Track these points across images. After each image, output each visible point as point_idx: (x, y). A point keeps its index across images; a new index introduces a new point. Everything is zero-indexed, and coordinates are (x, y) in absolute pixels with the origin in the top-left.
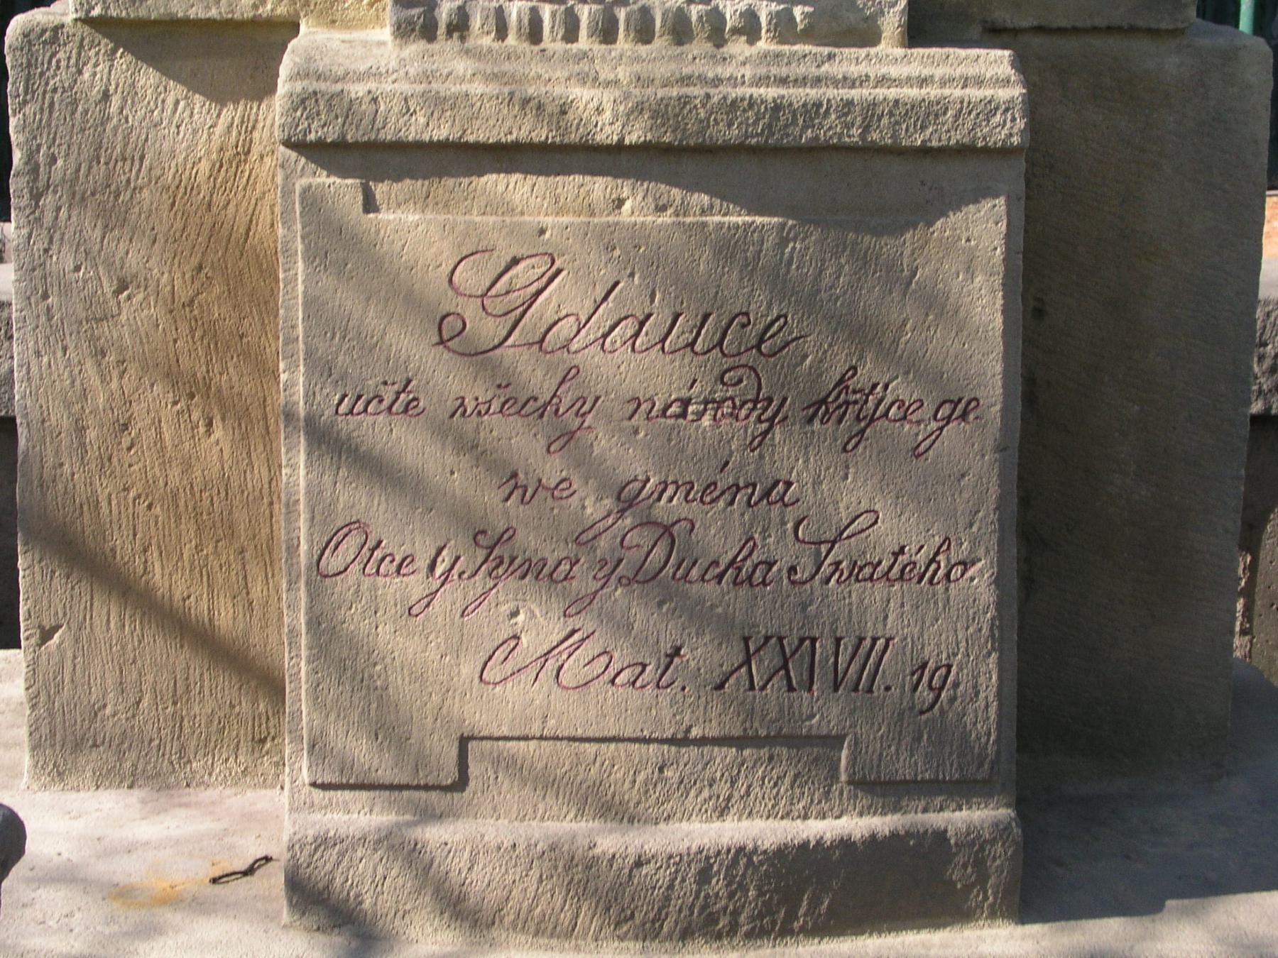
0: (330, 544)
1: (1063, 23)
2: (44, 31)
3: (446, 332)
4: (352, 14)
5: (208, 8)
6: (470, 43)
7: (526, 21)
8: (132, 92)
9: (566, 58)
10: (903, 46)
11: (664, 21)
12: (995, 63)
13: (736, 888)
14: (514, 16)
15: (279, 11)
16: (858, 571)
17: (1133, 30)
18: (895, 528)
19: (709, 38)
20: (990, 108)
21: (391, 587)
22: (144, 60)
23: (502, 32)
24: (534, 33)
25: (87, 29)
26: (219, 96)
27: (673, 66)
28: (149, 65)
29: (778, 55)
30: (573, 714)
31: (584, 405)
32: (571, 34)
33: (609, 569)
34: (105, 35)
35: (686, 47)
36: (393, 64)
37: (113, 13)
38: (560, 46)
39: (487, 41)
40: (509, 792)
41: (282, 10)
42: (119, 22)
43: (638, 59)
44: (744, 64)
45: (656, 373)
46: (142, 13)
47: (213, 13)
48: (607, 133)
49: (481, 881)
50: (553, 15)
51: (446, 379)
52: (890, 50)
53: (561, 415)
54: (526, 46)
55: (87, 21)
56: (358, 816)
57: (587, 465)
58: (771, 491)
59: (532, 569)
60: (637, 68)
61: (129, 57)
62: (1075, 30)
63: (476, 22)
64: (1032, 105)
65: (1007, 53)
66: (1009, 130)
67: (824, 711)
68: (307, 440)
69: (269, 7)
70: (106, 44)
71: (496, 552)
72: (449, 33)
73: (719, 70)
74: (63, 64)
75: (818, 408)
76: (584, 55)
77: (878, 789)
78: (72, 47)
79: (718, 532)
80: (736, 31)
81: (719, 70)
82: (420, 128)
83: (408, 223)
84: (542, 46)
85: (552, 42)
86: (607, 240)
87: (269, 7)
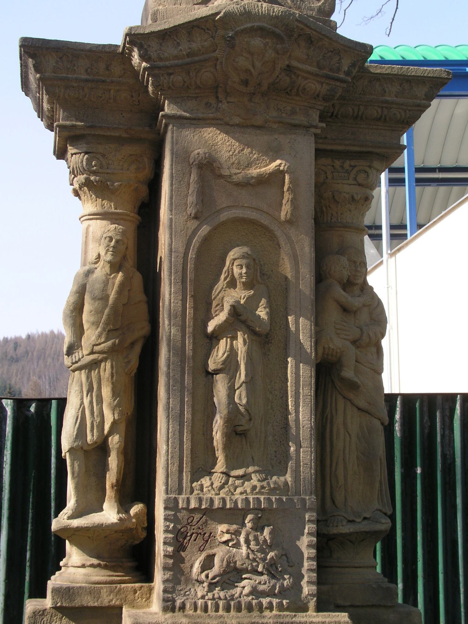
1: (359, 604)
2: (40, 611)
4: (139, 604)
5: (94, 603)
6: (186, 613)
7: (203, 606)
9: (217, 617)
10: (316, 612)
11: (245, 605)
14: (200, 604)
15: (116, 603)
17: (380, 606)
19: (258, 611)
22: (71, 620)
23: (196, 609)
24: (206, 610)
25: (54, 610)
27: (249, 619)
28: (73, 622)
29: (280, 615)
32: (217, 610)
34: (59, 612)
35: (252, 613)
36: (163, 620)
37: (64, 605)
38: (214, 614)
39: (191, 612)
41: (118, 603)
42: (65, 608)
43: (238, 617)
44: (270, 618)
46: (73, 605)
47: (96, 604)
50: (212, 604)
52: (312, 614)
54: (203, 614)
55: (55, 608)
60: (238, 620)
61: (67, 619)
62: (362, 606)
63: (188, 606)
65: (347, 614)
69: (114, 602)
70: (60, 615)
72: (179, 610)
73: (263, 620)
74: (45, 622)
76: (221, 616)
78: (49, 616)
80: (266, 608)
81: (263, 620)
84: (208, 614)
85: (211, 612)
87: (114, 602)
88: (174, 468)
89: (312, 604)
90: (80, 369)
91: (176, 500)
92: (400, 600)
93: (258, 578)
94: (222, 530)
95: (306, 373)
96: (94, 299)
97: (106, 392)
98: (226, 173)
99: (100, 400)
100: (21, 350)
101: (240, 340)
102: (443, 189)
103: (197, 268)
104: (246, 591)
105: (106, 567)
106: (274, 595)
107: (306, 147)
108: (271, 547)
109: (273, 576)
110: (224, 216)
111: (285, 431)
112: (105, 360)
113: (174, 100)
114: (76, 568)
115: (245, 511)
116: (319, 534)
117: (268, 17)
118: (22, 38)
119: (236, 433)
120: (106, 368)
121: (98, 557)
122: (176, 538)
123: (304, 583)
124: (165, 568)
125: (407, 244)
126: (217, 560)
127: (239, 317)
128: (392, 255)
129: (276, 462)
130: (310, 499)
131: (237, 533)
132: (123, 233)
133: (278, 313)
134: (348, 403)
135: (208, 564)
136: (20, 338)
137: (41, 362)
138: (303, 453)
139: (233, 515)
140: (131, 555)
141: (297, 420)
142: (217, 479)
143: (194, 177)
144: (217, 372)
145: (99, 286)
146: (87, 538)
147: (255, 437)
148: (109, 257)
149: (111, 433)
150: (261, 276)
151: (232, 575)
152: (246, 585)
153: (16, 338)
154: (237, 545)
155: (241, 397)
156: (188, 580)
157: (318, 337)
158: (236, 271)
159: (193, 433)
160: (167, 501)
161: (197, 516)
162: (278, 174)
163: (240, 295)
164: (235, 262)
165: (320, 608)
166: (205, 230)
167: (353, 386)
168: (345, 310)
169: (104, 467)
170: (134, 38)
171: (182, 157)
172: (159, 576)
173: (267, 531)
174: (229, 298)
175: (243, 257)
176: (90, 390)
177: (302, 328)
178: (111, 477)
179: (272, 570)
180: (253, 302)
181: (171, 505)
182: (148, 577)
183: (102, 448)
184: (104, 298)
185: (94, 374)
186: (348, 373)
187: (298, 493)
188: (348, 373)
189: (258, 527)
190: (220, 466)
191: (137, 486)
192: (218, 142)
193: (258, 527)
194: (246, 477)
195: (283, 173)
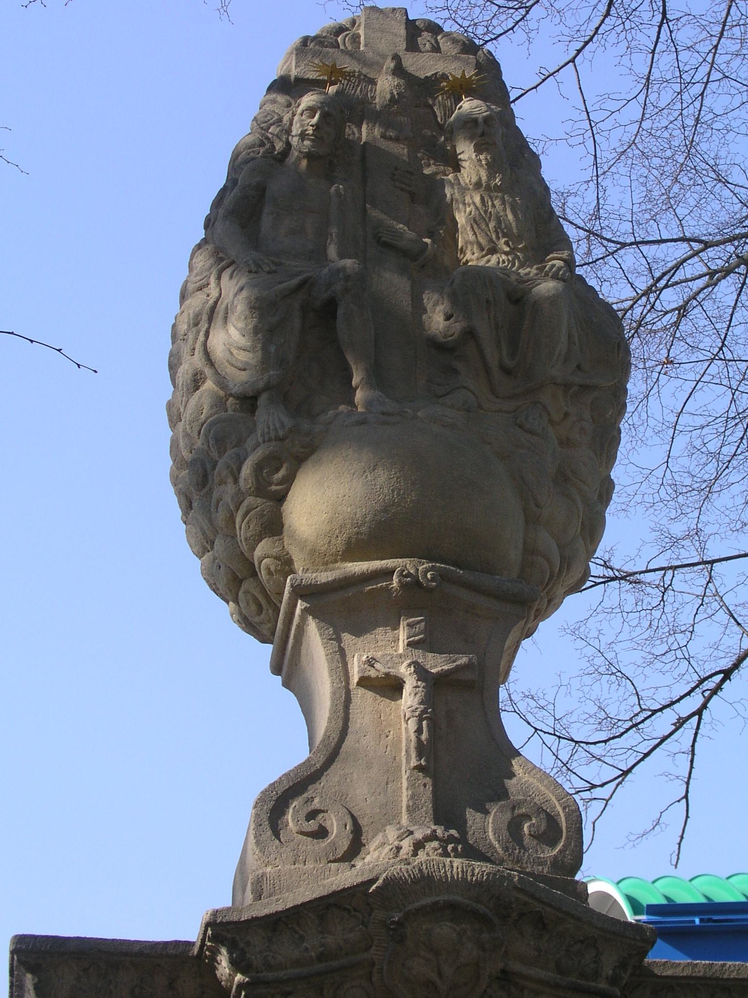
117: (463, 884)
118: (16, 936)
170: (220, 929)
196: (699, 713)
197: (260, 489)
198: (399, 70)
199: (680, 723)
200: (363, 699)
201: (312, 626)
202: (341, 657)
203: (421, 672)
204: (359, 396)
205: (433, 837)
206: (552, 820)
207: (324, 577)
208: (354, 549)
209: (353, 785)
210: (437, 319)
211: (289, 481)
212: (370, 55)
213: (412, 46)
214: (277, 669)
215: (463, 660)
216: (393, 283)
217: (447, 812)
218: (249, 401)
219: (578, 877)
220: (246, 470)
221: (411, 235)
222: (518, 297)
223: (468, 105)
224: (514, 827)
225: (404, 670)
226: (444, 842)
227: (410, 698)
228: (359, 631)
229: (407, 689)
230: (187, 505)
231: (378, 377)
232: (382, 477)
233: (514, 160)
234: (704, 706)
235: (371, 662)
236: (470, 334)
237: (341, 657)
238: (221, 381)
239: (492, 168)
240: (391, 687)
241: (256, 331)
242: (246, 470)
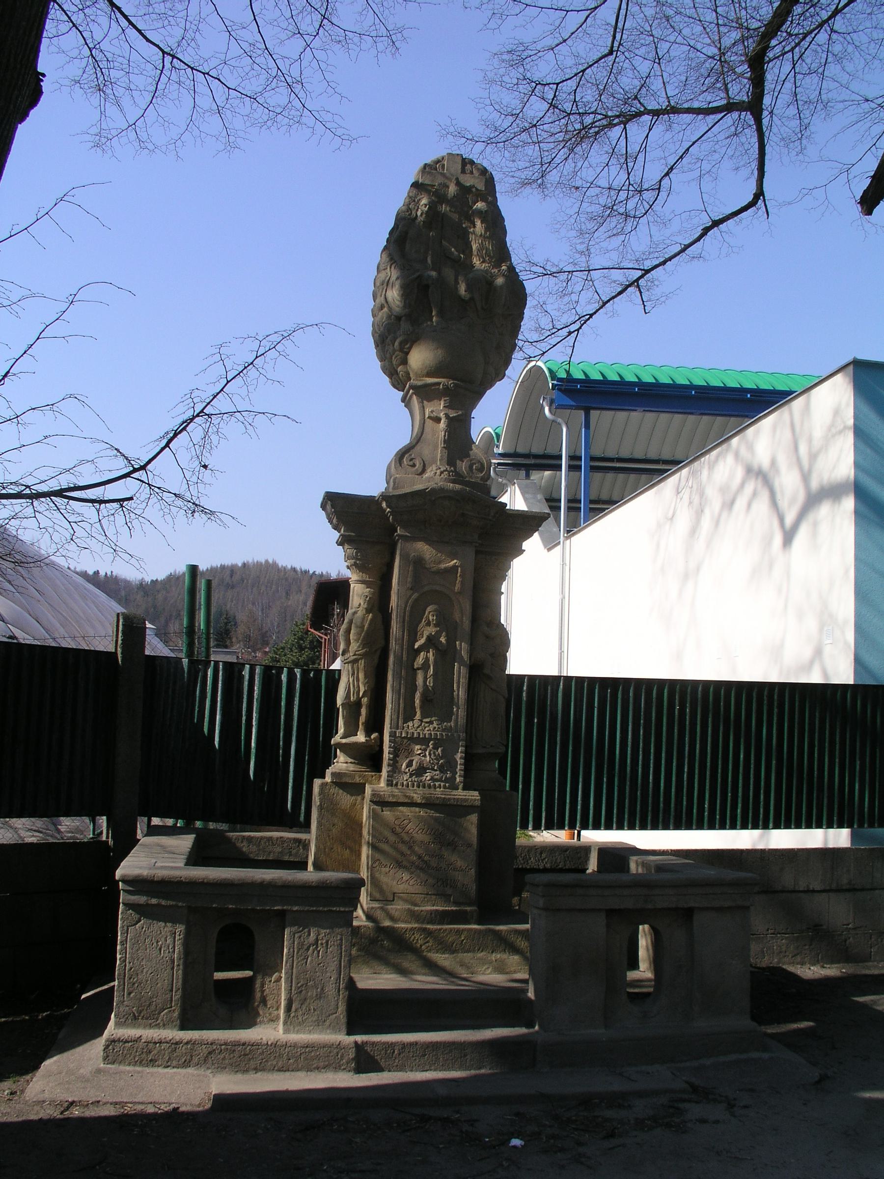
0: (375, 862)
3: (393, 831)
8: (338, 794)
12: (476, 793)
13: (436, 916)
16: (455, 869)
18: (459, 863)
20: (475, 800)
21: (383, 869)
26: (352, 795)
30: (411, 889)
31: (414, 842)
33: (417, 867)
40: (401, 903)
45: (420, 836)
48: (419, 801)
49: (397, 915)
51: (392, 838)
53: (410, 844)
55: (332, 782)
56: (376, 905)
57: (413, 852)
58: (441, 857)
59: (405, 867)
64: (481, 800)
66: (478, 803)
67: (449, 891)
68: (523, 494)
71: (400, 865)
75: (449, 844)
77: (456, 903)
79: (434, 863)
82: (391, 799)
83: (387, 814)
86: (418, 817)
88: (394, 717)
89: (461, 786)
90: (348, 663)
91: (395, 732)
92: (508, 788)
93: (435, 773)
94: (417, 749)
95: (464, 671)
96: (357, 627)
97: (361, 676)
98: (428, 566)
99: (358, 680)
100: (237, 577)
101: (431, 653)
102: (621, 476)
103: (412, 607)
104: (428, 778)
105: (358, 764)
106: (442, 781)
107: (470, 553)
108: (441, 758)
109: (441, 772)
110: (426, 589)
111: (452, 701)
112: (361, 659)
113: (403, 527)
114: (341, 763)
115: (430, 739)
116: (466, 752)
117: (452, 491)
118: (327, 493)
119: (427, 700)
120: (362, 663)
121: (354, 759)
122: (394, 751)
123: (457, 776)
124: (389, 765)
125: (579, 531)
126: (414, 763)
127: (432, 641)
128: (567, 538)
129: (446, 716)
130: (463, 735)
131: (425, 750)
132: (373, 594)
133: (451, 641)
134: (765, 495)
135: (410, 764)
136: (236, 565)
137: (255, 589)
138: (460, 713)
139: (423, 741)
140: (370, 758)
141: (458, 695)
142: (416, 723)
143: (411, 568)
144: (418, 669)
145: (359, 620)
146: (348, 749)
147: (436, 703)
148: (365, 606)
149: (363, 697)
150: (444, 621)
151: (421, 770)
152: (428, 776)
153: (233, 566)
154: (425, 756)
155: (430, 682)
156: (400, 772)
157: (471, 653)
158: (431, 618)
159: (405, 699)
160: (390, 733)
161: (405, 741)
162: (455, 567)
163: (431, 630)
164: (430, 613)
165: (464, 789)
166: (415, 595)
167: (489, 678)
168: (487, 637)
169: (359, 714)
170: (384, 497)
171: (405, 558)
172: (385, 770)
173: (440, 750)
174: (427, 631)
175: (434, 611)
176: (353, 674)
177: (463, 647)
178: (362, 719)
179: (442, 769)
180: (438, 634)
181: (392, 735)
182: (379, 770)
183: (358, 704)
184: (362, 627)
185: (355, 666)
186: (487, 671)
187: (457, 732)
188: (487, 671)
189: (436, 748)
190: (418, 716)
191: (375, 724)
192: (424, 549)
193: (436, 748)
194: (431, 723)
195: (457, 567)
196: (578, 330)
197: (401, 350)
198: (458, 183)
199: (570, 333)
200: (429, 423)
201: (414, 397)
202: (423, 409)
203: (447, 416)
204: (434, 319)
205: (446, 470)
206: (482, 465)
207: (419, 383)
208: (429, 374)
209: (425, 450)
210: (462, 289)
211: (410, 348)
212: (448, 175)
213: (463, 171)
214: (403, 400)
215: (460, 413)
216: (449, 273)
217: (451, 462)
218: (398, 318)
219: (488, 483)
220: (397, 344)
221: (456, 253)
222: (489, 283)
223: (480, 205)
224: (471, 467)
225: (442, 415)
226: (449, 472)
227: (443, 425)
228: (429, 401)
229: (442, 421)
230: (377, 346)
231: (441, 314)
232: (440, 351)
233: (495, 223)
234: (580, 328)
235: (432, 412)
236: (472, 299)
237: (423, 409)
238: (390, 308)
239: (486, 229)
240: (438, 420)
241: (402, 295)
242: (397, 344)
